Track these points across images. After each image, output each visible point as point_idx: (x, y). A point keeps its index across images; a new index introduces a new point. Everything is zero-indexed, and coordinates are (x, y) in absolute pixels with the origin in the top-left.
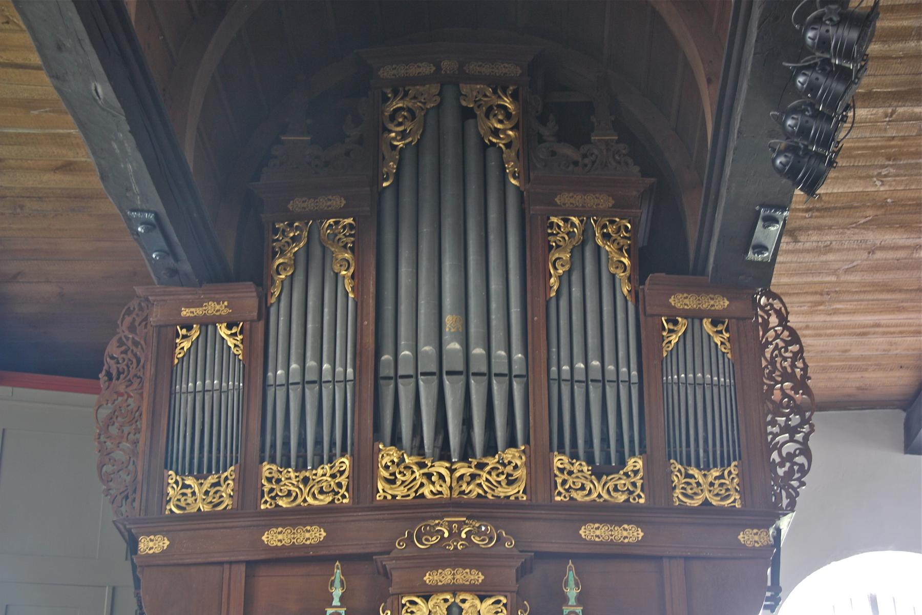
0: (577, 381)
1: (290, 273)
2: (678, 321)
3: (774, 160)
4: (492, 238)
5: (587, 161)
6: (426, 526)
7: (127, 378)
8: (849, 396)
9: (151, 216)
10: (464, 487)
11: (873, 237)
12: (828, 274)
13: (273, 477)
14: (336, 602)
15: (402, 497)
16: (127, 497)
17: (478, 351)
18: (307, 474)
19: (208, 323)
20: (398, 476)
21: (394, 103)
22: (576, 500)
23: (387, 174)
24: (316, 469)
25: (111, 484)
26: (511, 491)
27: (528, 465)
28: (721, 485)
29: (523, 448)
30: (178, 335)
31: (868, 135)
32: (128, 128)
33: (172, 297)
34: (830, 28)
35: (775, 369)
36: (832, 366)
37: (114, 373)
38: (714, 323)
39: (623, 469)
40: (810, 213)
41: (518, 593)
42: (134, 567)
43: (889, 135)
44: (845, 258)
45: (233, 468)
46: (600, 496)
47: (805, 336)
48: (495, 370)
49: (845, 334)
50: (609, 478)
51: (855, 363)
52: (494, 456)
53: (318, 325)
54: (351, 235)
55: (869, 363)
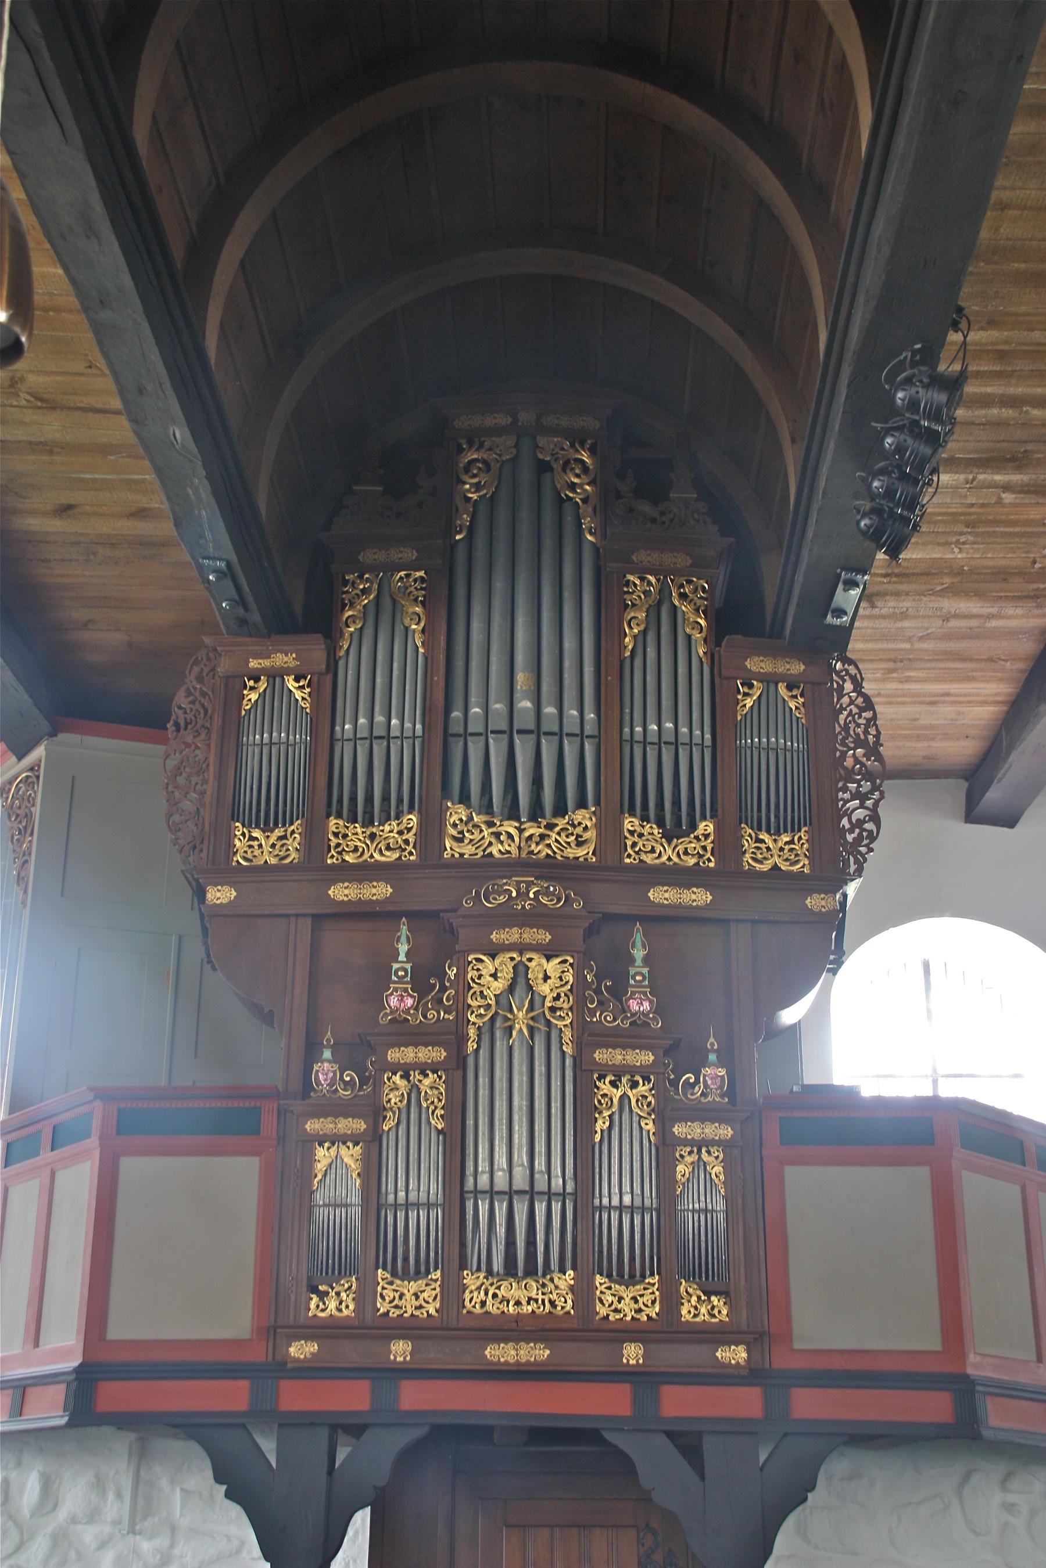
0: (650, 743)
1: (359, 626)
2: (753, 685)
3: (858, 522)
4: (567, 595)
5: (664, 518)
6: (494, 885)
7: (195, 729)
8: (916, 765)
9: (223, 565)
10: (533, 847)
11: (949, 605)
12: (903, 641)
13: (340, 832)
14: (402, 957)
15: (470, 855)
16: (194, 847)
17: (549, 710)
18: (374, 830)
19: (275, 675)
20: (467, 834)
21: (469, 454)
22: (645, 862)
23: (461, 526)
24: (383, 826)
25: (180, 834)
26: (581, 852)
27: (598, 826)
28: (791, 850)
29: (593, 809)
30: (739, 692)
31: (948, 501)
32: (204, 473)
33: (240, 648)
34: (920, 390)
35: (848, 735)
36: (900, 735)
37: (182, 723)
38: (789, 688)
39: (693, 833)
40: (888, 579)
41: (584, 954)
42: (202, 917)
43: (969, 502)
44: (920, 625)
45: (299, 822)
46: (669, 859)
47: (877, 703)
48: (566, 730)
49: (915, 703)
50: (680, 841)
51: (923, 732)
52: (564, 817)
53: (387, 680)
54: (422, 589)
55: (937, 732)
